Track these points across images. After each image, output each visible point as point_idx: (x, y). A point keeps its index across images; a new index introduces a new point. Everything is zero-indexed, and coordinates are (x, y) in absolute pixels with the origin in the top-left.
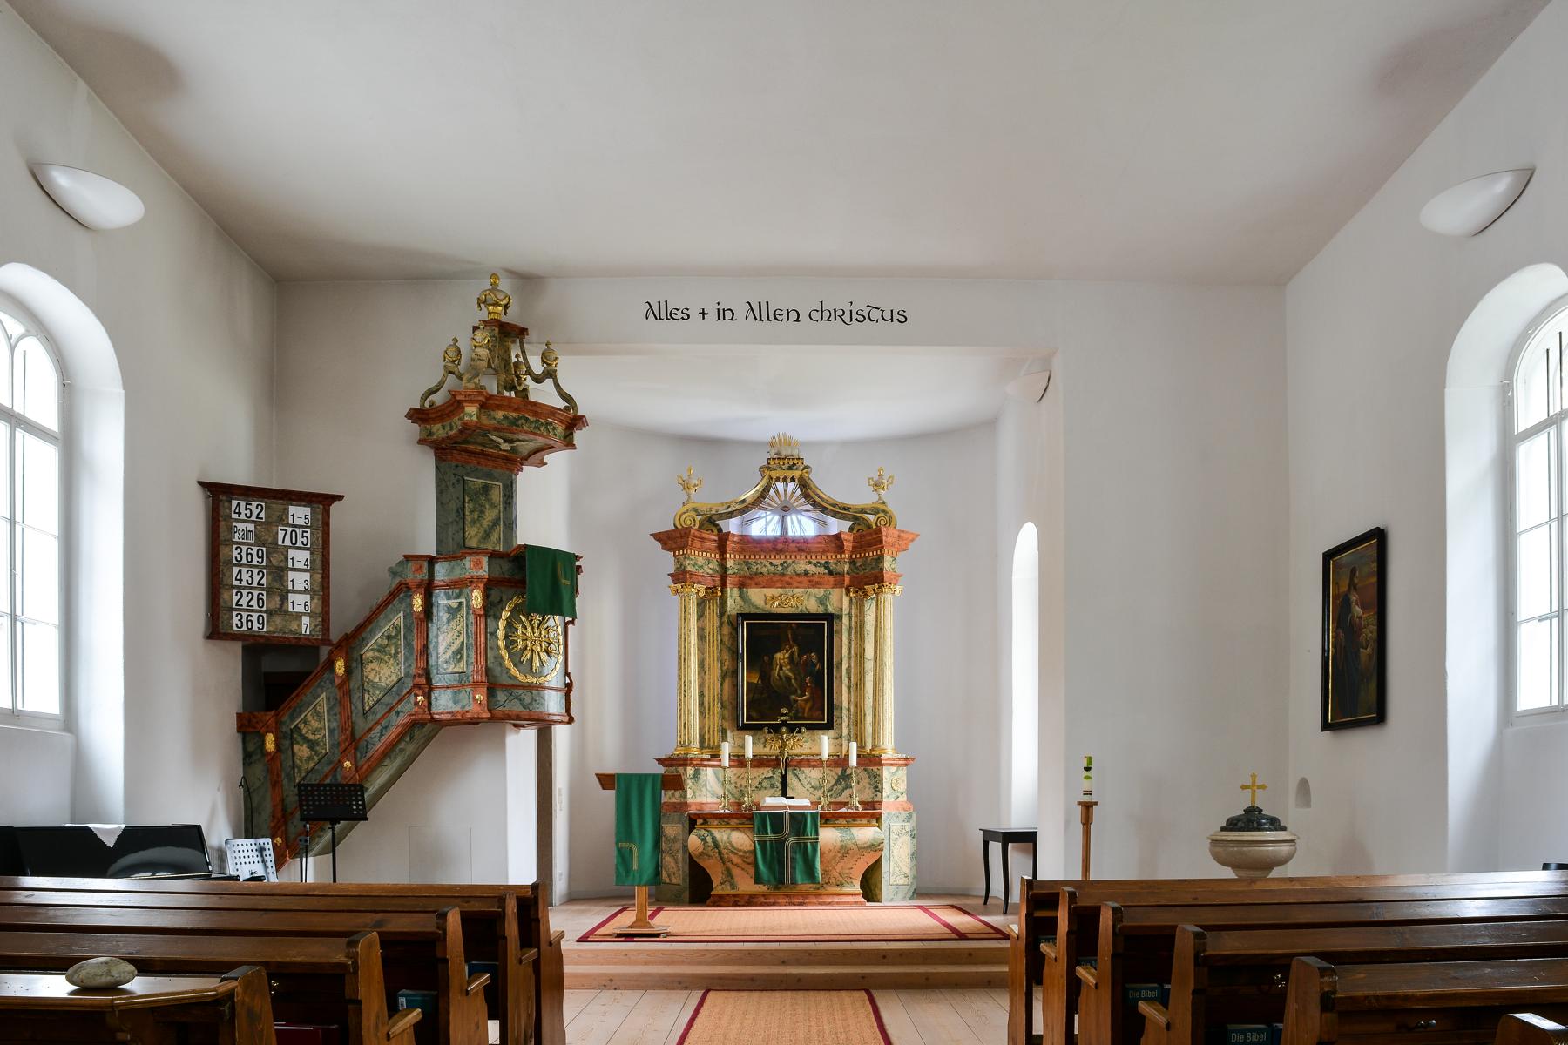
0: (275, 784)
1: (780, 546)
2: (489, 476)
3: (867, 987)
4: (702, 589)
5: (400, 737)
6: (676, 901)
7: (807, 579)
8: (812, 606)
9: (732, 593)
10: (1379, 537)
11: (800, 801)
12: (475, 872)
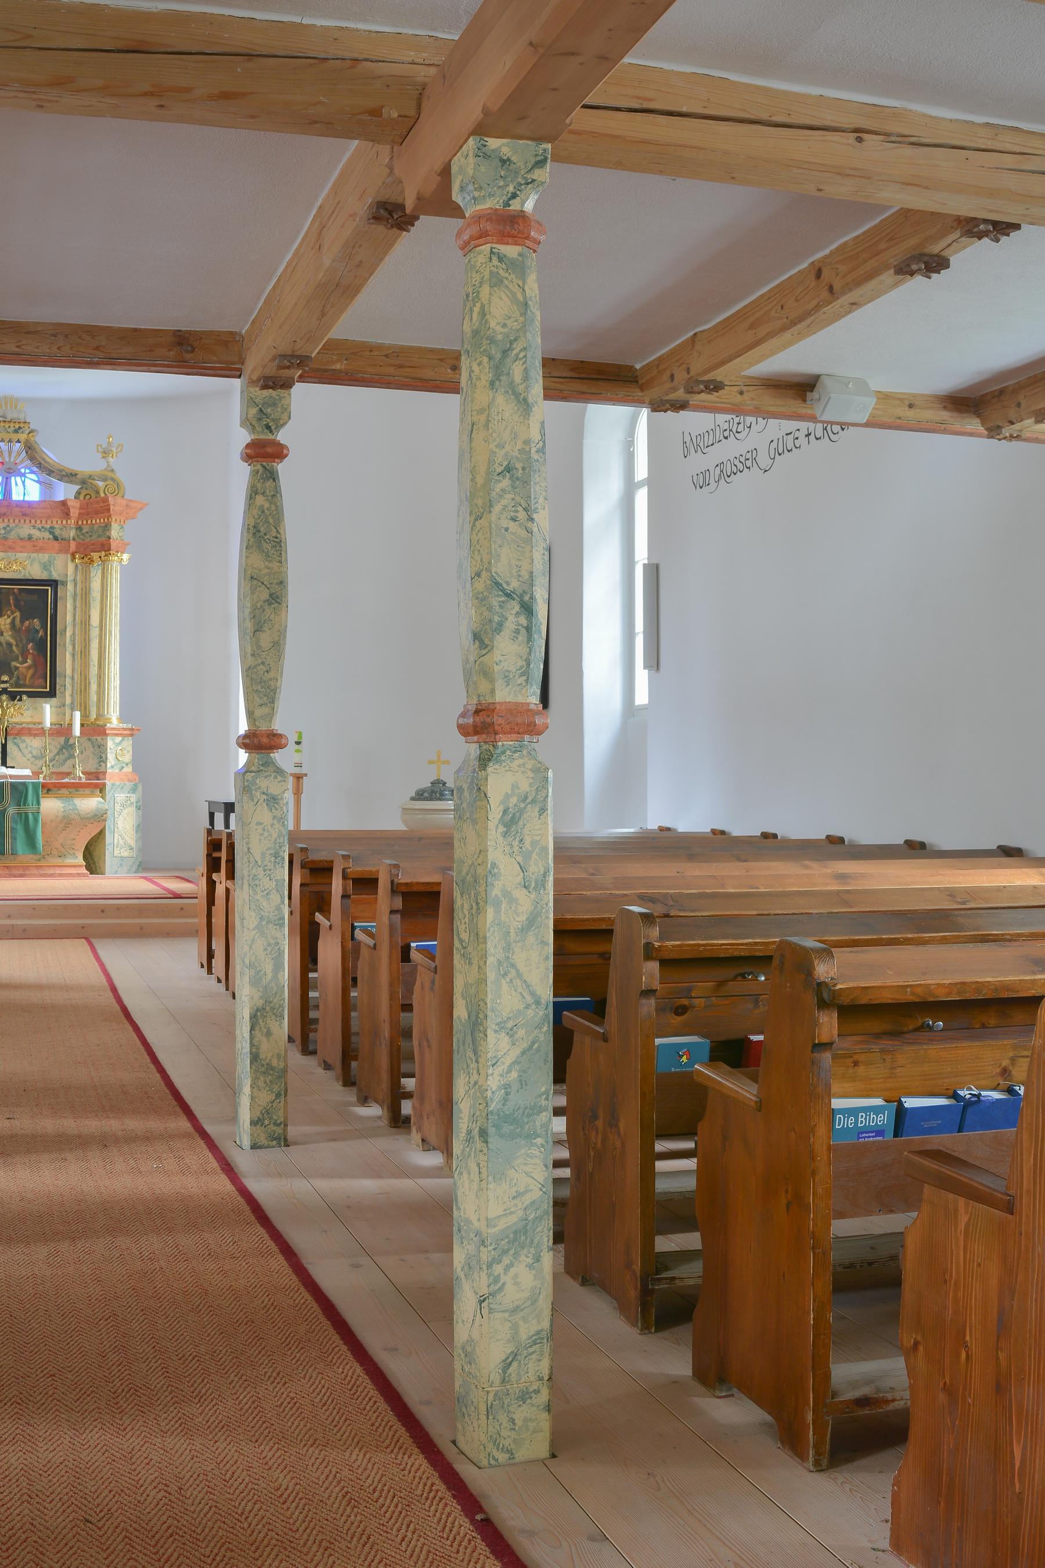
3: (87, 936)
7: (31, 544)
8: (36, 572)
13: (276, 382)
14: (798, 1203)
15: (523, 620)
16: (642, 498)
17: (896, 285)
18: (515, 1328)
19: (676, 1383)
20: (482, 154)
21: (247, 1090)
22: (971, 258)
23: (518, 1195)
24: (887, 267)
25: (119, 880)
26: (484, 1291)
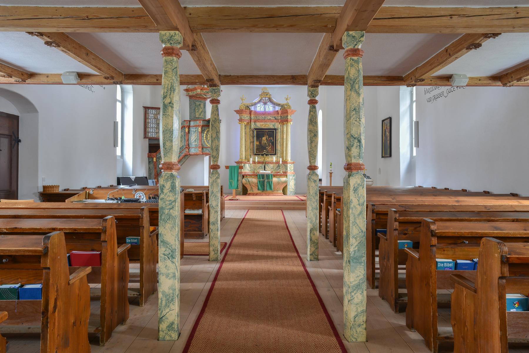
0: (155, 168)
1: (264, 113)
2: (201, 102)
3: (282, 209)
4: (246, 123)
5: (183, 158)
6: (239, 194)
7: (271, 121)
9: (253, 124)
10: (390, 118)
11: (268, 172)
12: (205, 185)
13: (315, 85)
14: (428, 284)
15: (358, 144)
16: (414, 104)
17: (467, 52)
18: (357, 308)
19: (402, 326)
20: (348, 35)
21: (309, 247)
22: (487, 44)
23: (358, 277)
24: (464, 48)
25: (290, 197)
26: (349, 299)
